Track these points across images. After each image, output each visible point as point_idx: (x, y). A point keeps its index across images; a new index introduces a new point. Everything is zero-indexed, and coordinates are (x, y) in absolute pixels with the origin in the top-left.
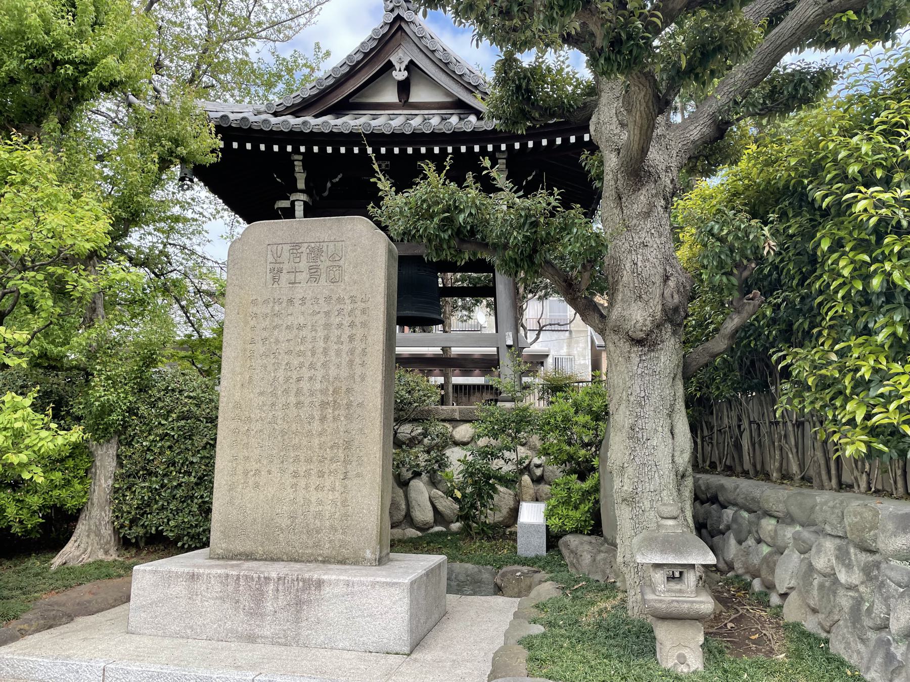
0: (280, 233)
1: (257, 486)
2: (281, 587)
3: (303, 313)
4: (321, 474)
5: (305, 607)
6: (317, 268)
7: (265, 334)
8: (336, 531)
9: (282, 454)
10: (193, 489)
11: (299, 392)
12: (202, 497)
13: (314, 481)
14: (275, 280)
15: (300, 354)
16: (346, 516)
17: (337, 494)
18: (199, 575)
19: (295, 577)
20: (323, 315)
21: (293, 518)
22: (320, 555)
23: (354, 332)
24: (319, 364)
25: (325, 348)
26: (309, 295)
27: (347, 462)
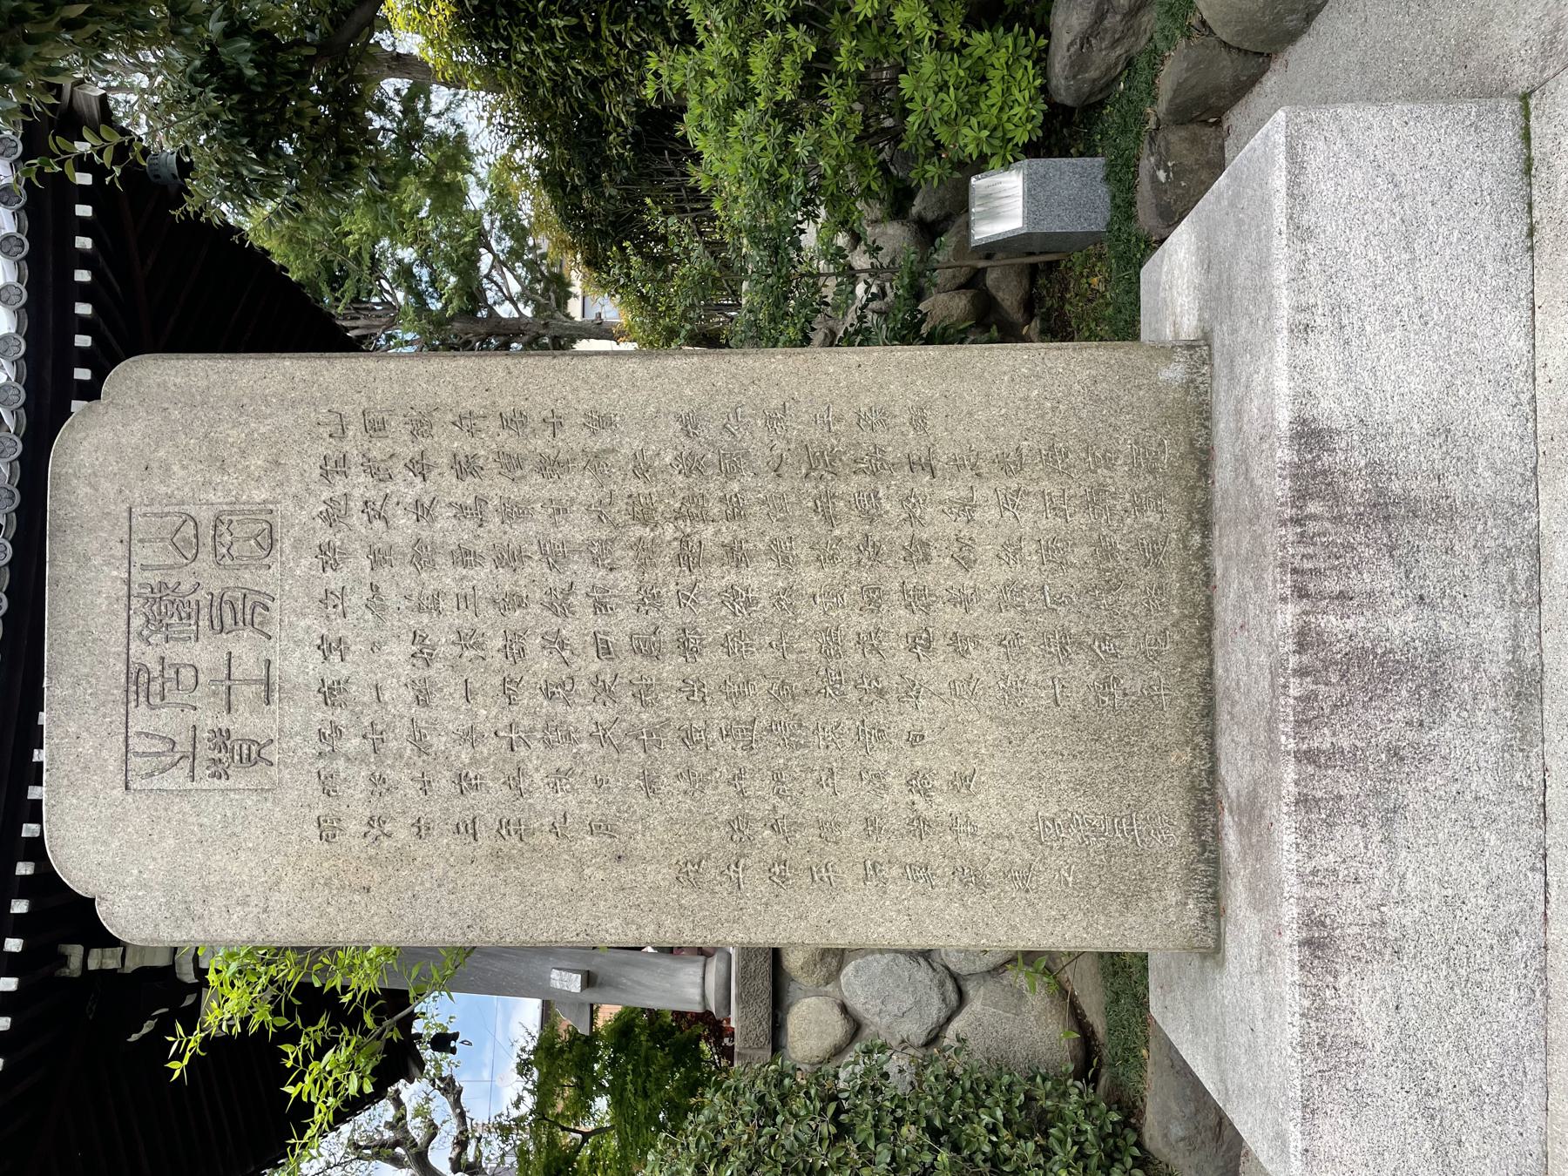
0: (87, 747)
1: (962, 783)
2: (1332, 585)
3: (375, 647)
4: (918, 552)
5: (1396, 486)
6: (219, 601)
7: (444, 783)
8: (1101, 488)
9: (853, 696)
10: (971, 1159)
11: (647, 648)
12: (993, 1130)
13: (939, 575)
14: (254, 756)
15: (514, 648)
16: (1052, 457)
17: (982, 492)
18: (1311, 920)
19: (1291, 533)
20: (385, 571)
21: (1065, 644)
22: (1184, 540)
23: (445, 460)
24: (553, 579)
25: (499, 562)
26: (312, 625)
27: (877, 466)
